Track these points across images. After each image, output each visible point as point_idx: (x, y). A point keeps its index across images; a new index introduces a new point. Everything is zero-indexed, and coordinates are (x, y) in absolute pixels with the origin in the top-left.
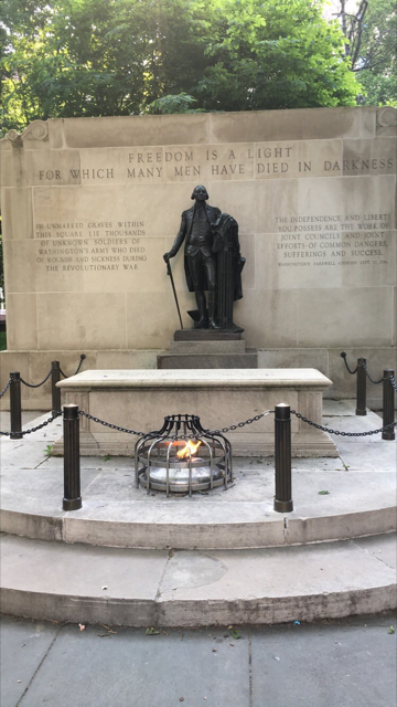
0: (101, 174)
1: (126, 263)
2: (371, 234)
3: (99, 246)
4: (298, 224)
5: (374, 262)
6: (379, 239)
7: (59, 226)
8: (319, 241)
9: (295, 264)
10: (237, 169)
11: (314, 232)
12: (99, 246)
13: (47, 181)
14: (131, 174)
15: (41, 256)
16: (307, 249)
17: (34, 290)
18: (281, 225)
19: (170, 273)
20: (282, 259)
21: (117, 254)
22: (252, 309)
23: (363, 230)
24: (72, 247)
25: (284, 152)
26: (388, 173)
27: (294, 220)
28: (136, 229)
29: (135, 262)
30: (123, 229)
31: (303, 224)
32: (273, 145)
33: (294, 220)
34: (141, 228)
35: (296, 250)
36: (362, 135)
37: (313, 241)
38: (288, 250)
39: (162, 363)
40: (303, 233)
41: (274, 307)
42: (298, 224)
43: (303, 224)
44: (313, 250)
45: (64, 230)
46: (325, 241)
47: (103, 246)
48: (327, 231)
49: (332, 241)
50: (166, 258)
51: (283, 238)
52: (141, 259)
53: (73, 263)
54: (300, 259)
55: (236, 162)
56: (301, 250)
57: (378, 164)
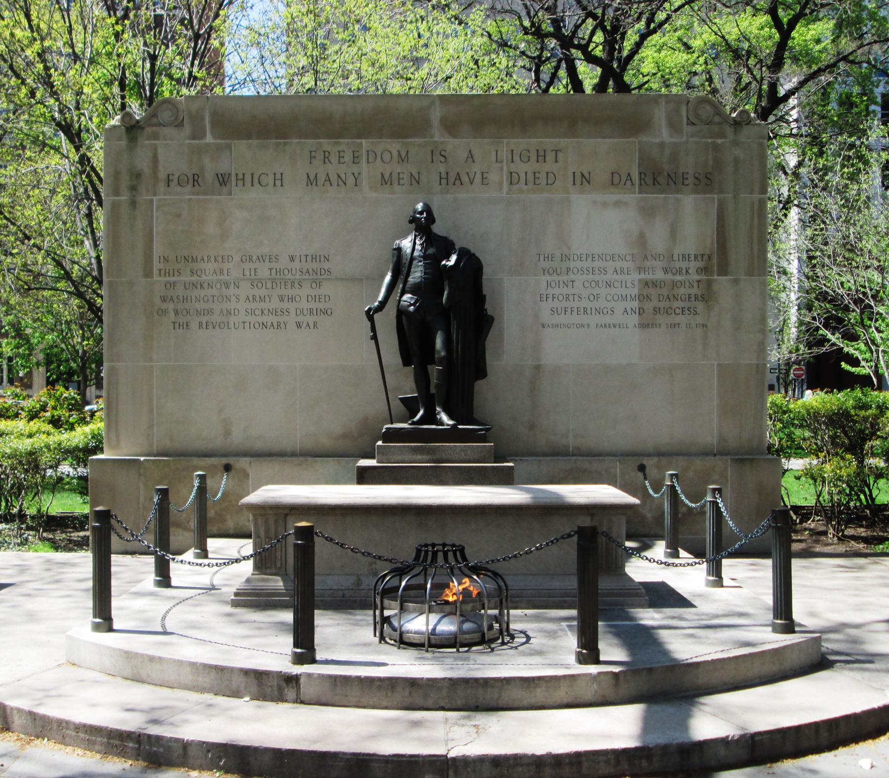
0: (264, 179)
1: (301, 318)
2: (682, 284)
3: (257, 292)
4: (572, 265)
5: (688, 326)
6: (695, 291)
7: (195, 260)
8: (603, 291)
9: (567, 326)
10: (478, 178)
11: (596, 277)
12: (257, 292)
13: (179, 189)
14: (311, 181)
15: (164, 306)
16: (585, 303)
17: (151, 360)
18: (546, 264)
19: (375, 338)
20: (546, 316)
21: (286, 305)
22: (496, 394)
23: (669, 277)
24: (214, 292)
25: (550, 157)
26: (705, 193)
27: (565, 258)
28: (317, 271)
29: (315, 318)
30: (296, 265)
31: (579, 264)
32: (533, 143)
33: (565, 258)
34: (326, 265)
35: (570, 304)
36: (665, 135)
37: (596, 291)
38: (556, 304)
39: (364, 477)
40: (579, 278)
41: (534, 388)
42: (572, 265)
43: (579, 264)
44: (595, 304)
45: (203, 265)
46: (613, 291)
47: (263, 292)
48: (616, 277)
49: (624, 292)
50: (370, 315)
51: (549, 284)
52: (325, 312)
53: (216, 318)
54: (575, 319)
55: (477, 168)
56: (575, 305)
57: (691, 180)
